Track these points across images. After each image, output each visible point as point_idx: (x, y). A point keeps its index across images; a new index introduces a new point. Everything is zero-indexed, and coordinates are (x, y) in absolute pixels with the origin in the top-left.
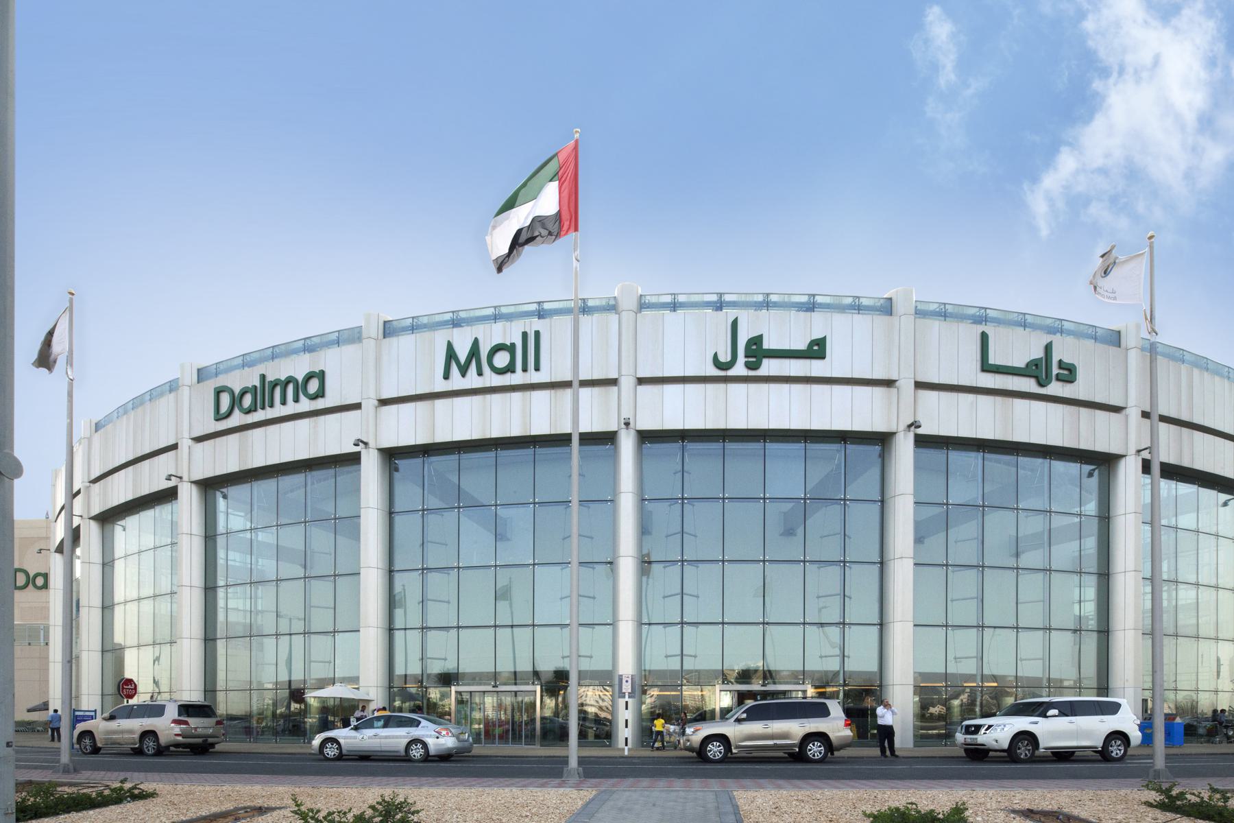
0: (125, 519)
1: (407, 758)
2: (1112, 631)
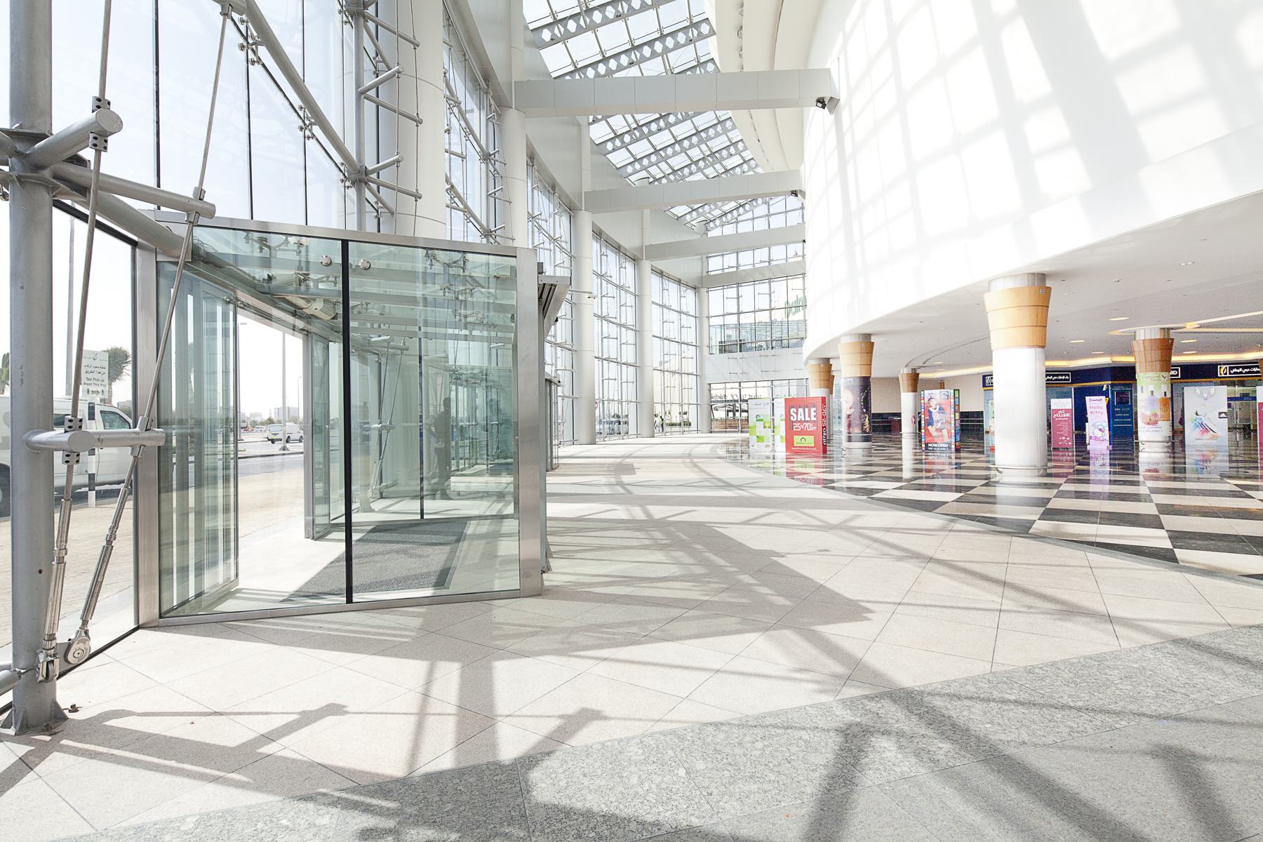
2: (498, 745)
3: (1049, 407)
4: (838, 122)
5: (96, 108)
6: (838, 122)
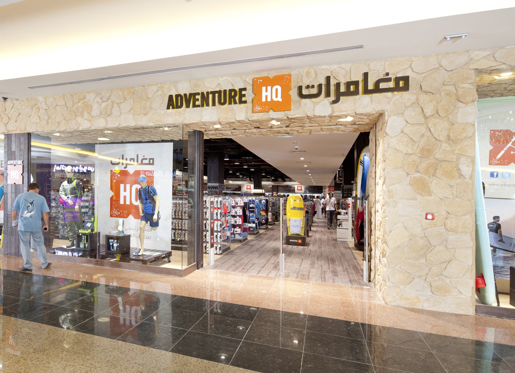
1: (78, 249)
4: (9, 98)
6: (9, 98)
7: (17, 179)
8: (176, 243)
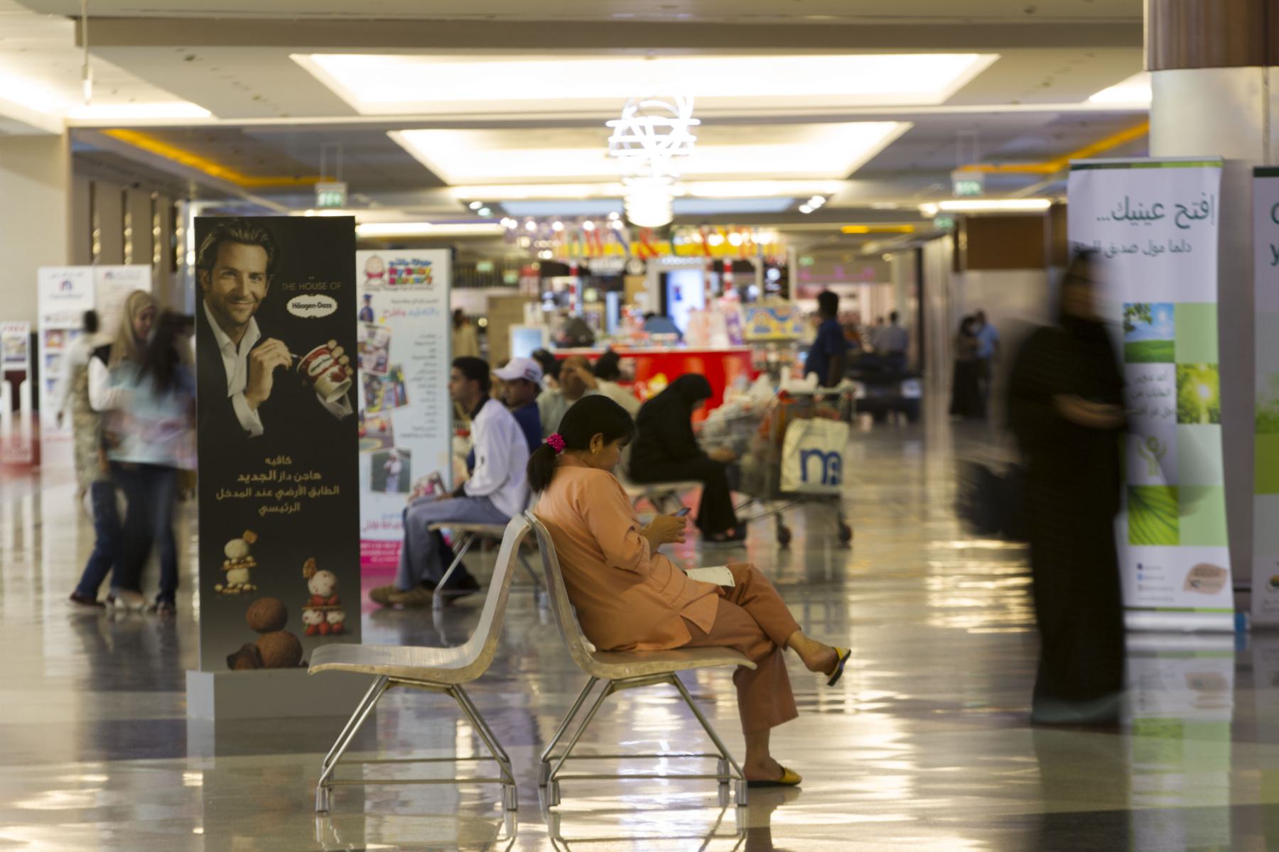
0: (310, 317)
2: (78, 652)
3: (508, 596)
5: (626, 180)
7: (253, 549)
8: (655, 679)
